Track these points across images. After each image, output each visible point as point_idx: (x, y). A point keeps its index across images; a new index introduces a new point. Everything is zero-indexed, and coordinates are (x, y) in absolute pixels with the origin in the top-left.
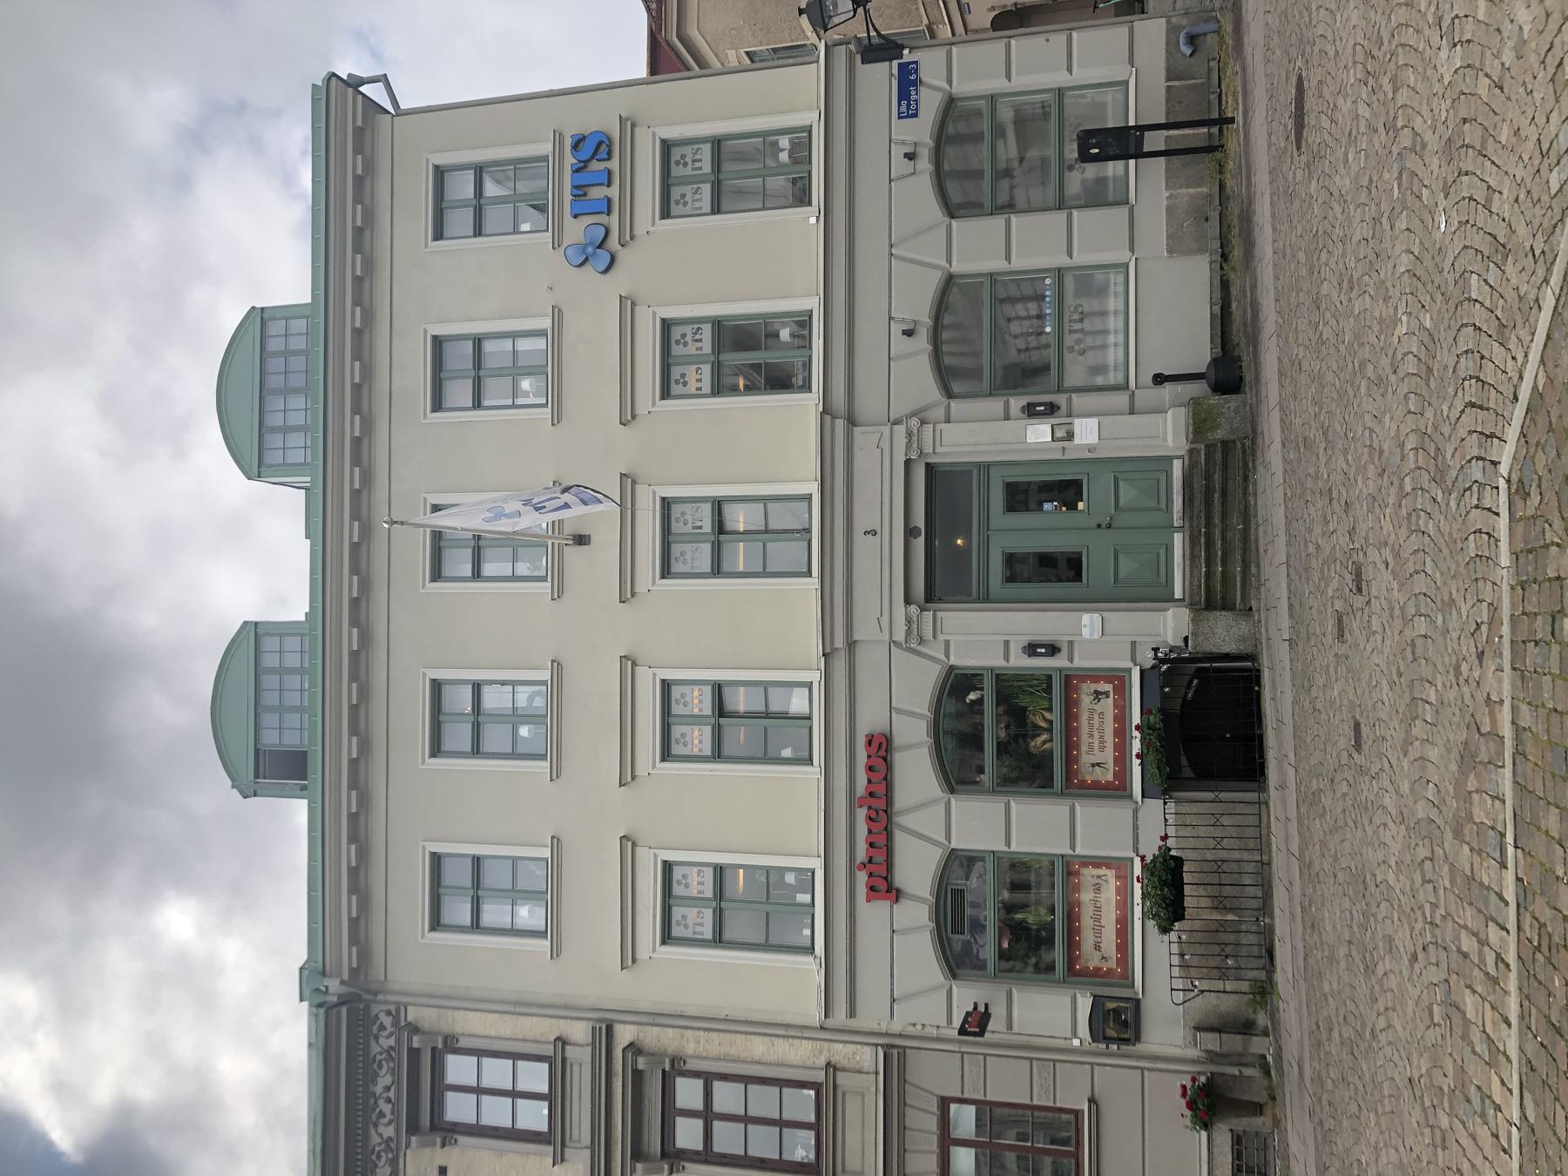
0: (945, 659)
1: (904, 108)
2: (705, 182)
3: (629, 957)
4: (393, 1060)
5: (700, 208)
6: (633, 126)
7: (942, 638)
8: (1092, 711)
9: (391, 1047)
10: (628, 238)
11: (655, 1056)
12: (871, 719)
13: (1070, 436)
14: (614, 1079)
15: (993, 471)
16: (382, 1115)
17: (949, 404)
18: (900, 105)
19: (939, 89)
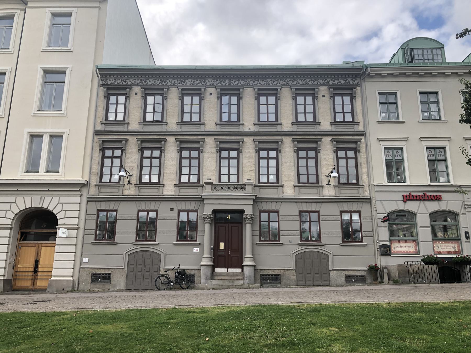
2: (435, 157)
3: (379, 140)
4: (267, 85)
5: (387, 157)
6: (449, 140)
7: (467, 213)
8: (451, 246)
9: (350, 83)
10: (422, 139)
11: (164, 145)
12: (444, 196)
14: (351, 136)
16: (334, 81)
19: (418, 211)
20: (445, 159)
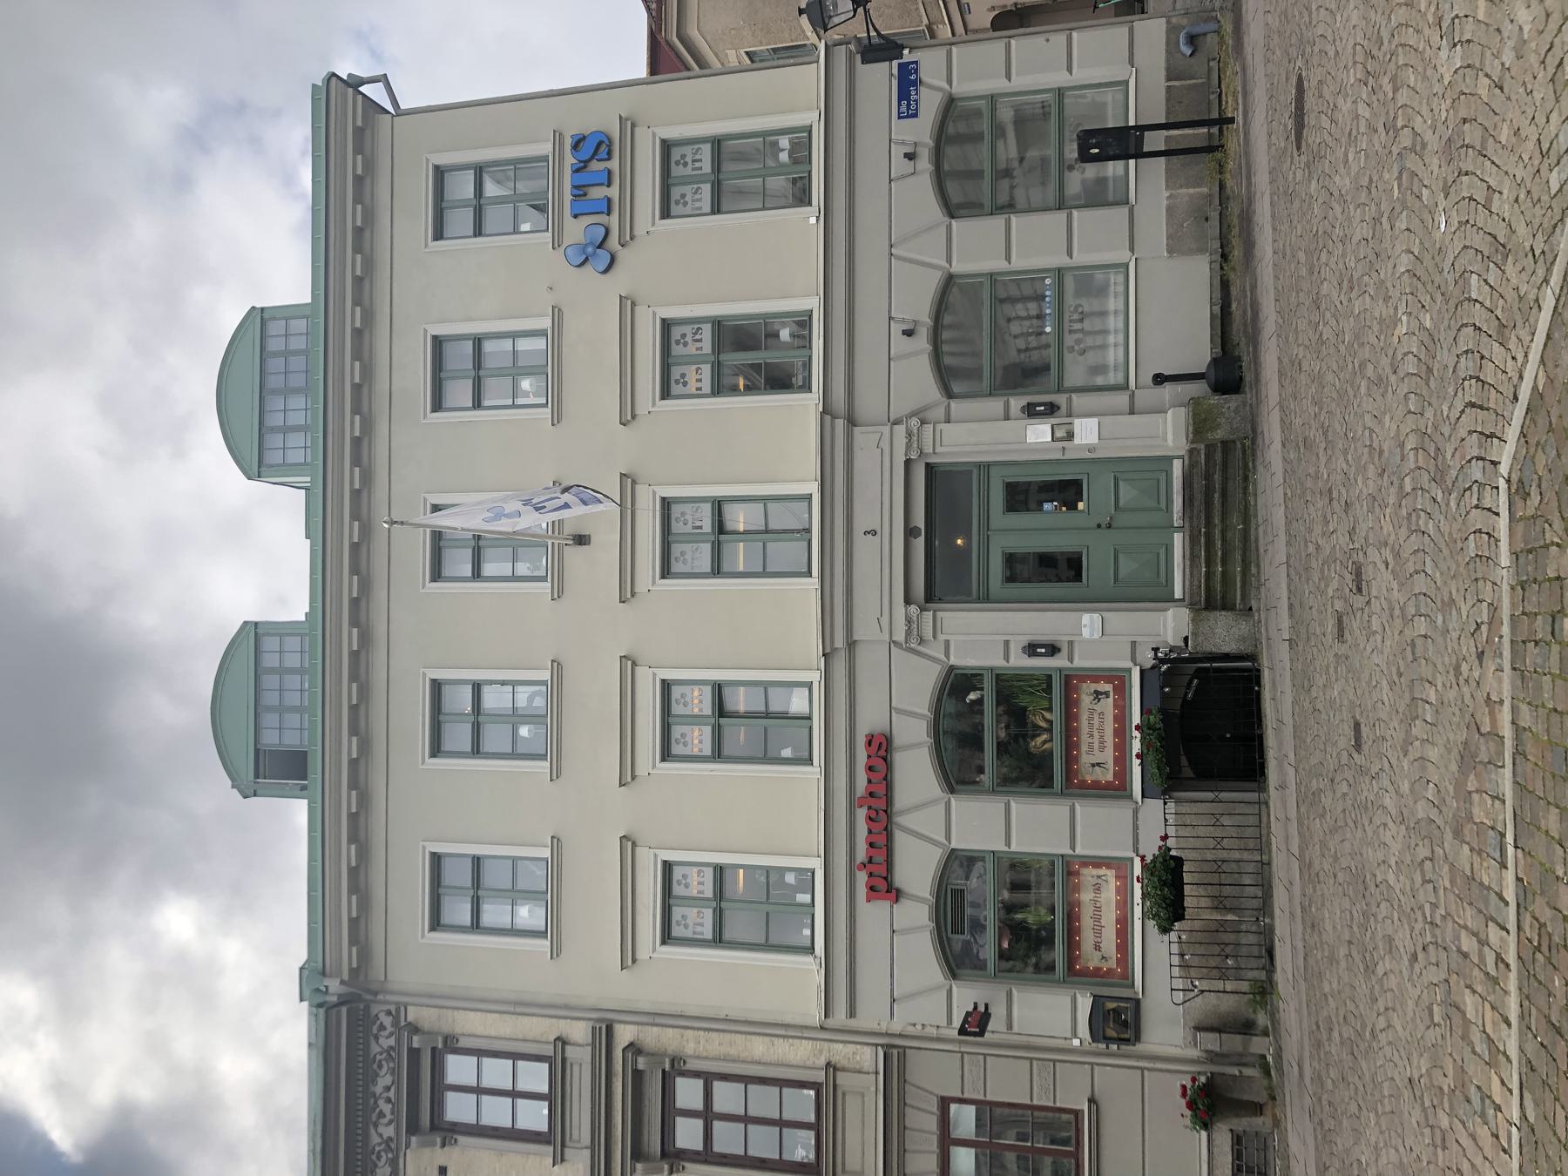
0: (945, 659)
1: (904, 108)
2: (705, 182)
3: (629, 957)
4: (393, 1060)
5: (700, 208)
6: (633, 126)
7: (942, 638)
8: (1092, 711)
9: (391, 1047)
10: (628, 238)
11: (655, 1056)
12: (871, 719)
13: (1070, 436)
14: (614, 1079)
15: (993, 471)
16: (382, 1115)
17: (949, 404)
18: (900, 105)
20: (715, 868)
